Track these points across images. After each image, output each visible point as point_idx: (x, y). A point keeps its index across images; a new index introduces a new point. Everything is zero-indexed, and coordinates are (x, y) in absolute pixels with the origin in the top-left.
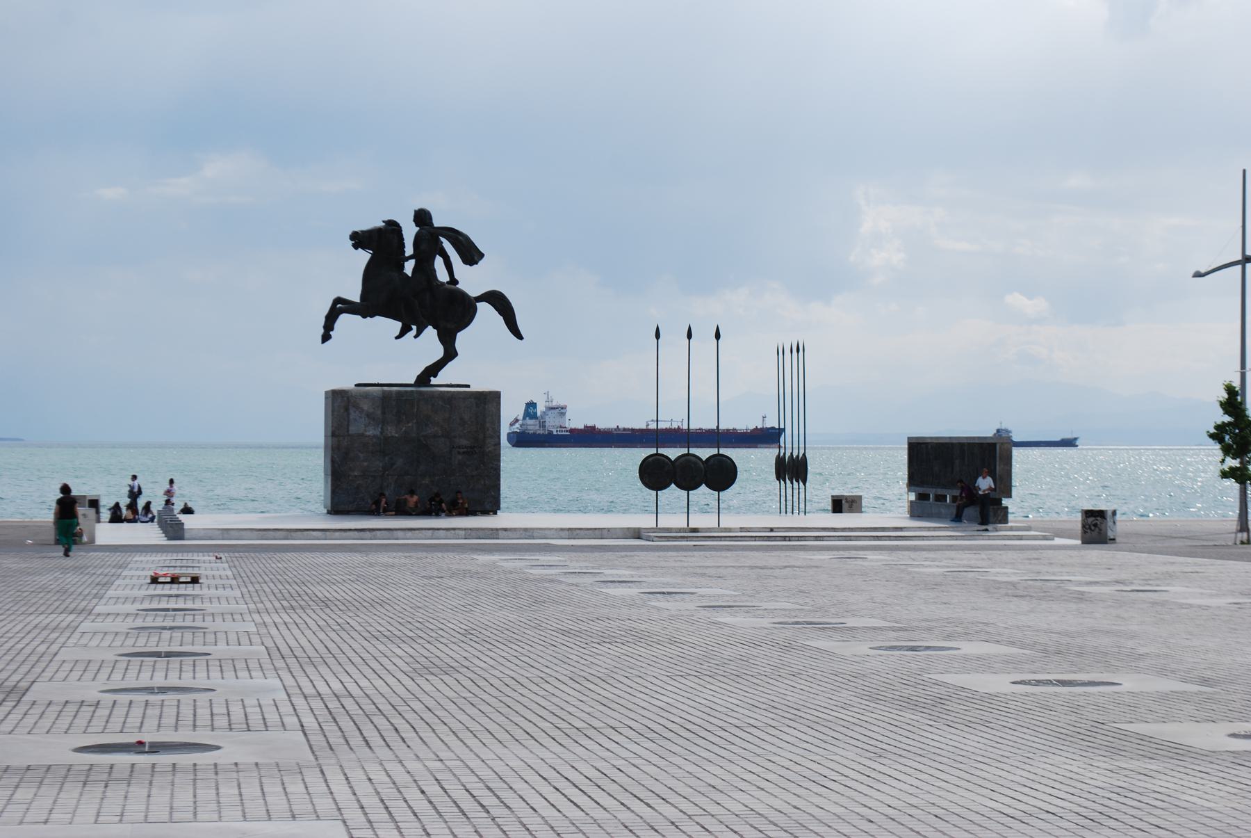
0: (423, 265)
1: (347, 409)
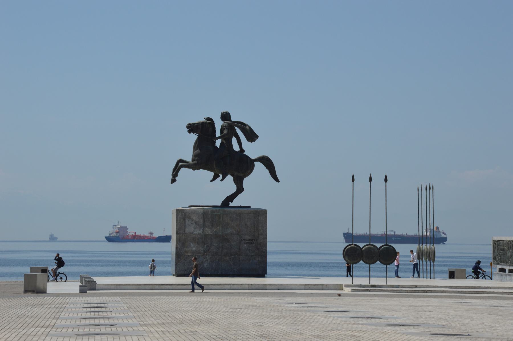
1: (184, 220)
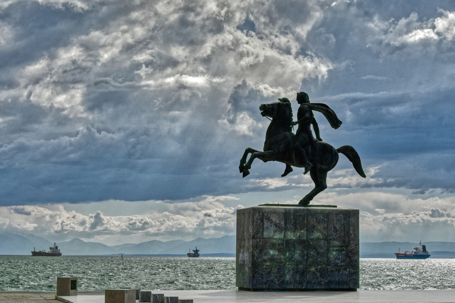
0: (304, 128)
1: (262, 221)
